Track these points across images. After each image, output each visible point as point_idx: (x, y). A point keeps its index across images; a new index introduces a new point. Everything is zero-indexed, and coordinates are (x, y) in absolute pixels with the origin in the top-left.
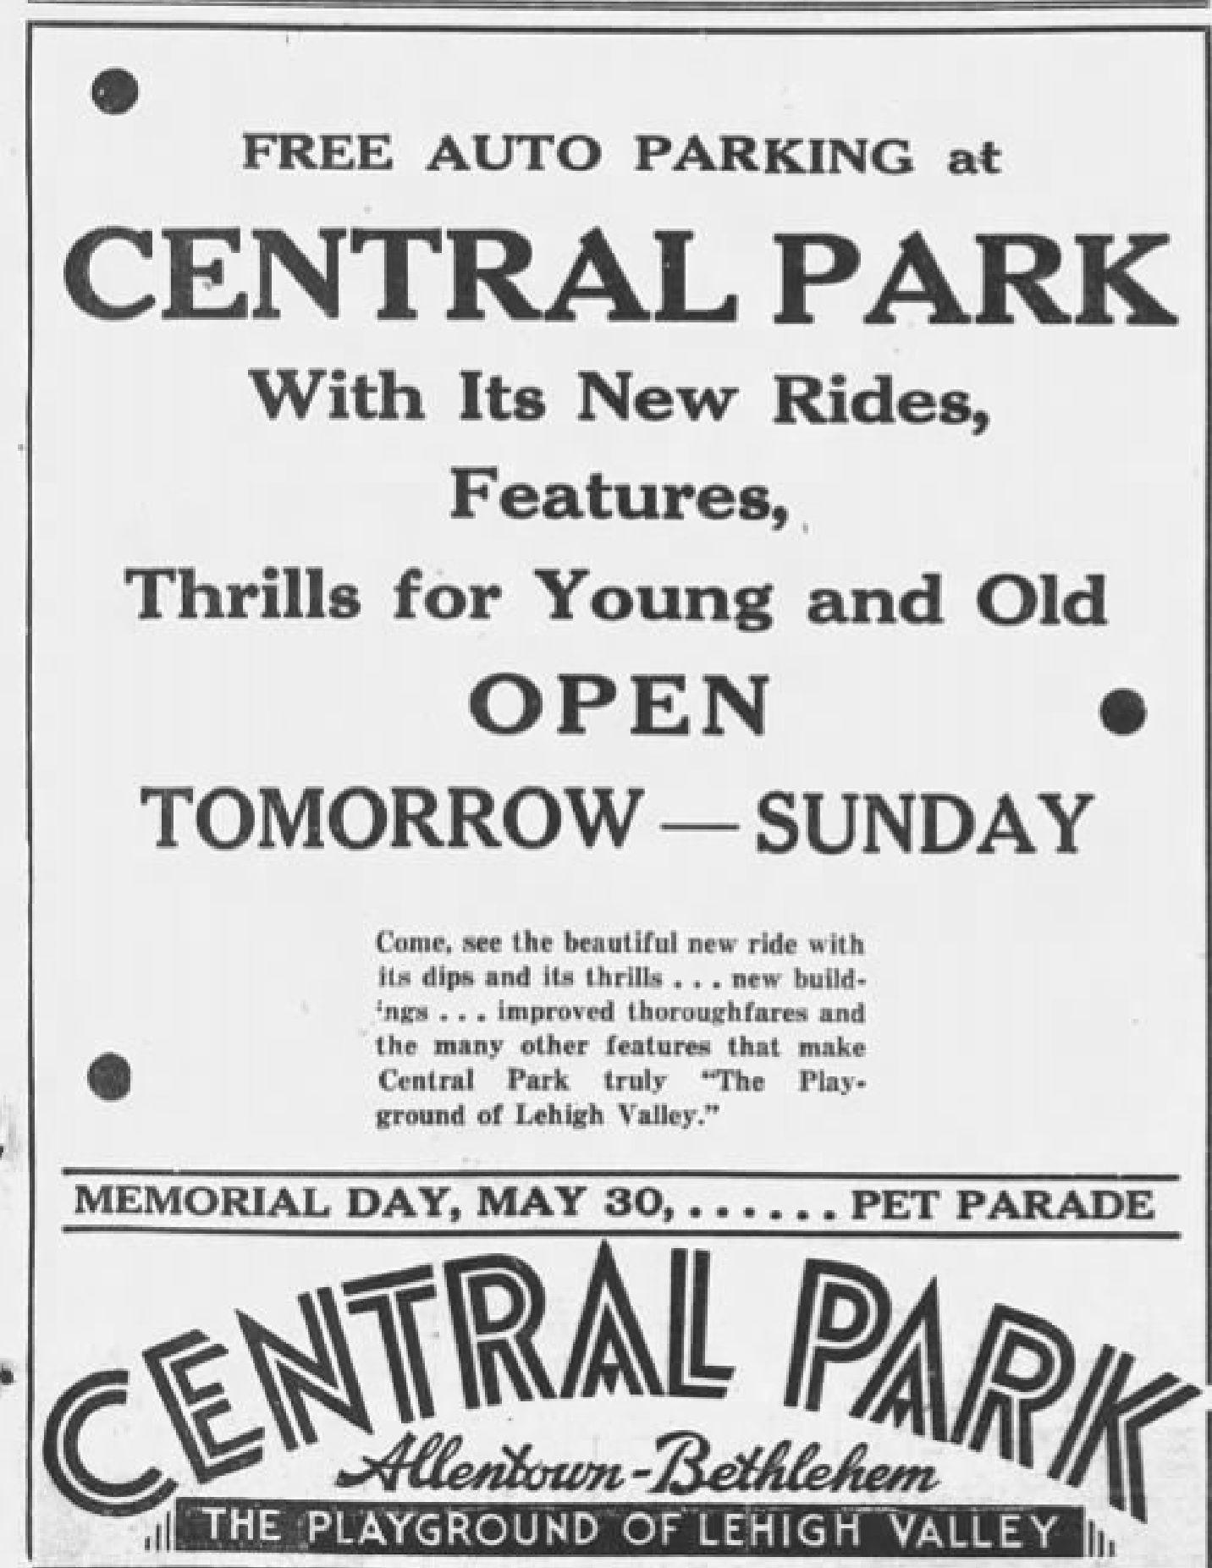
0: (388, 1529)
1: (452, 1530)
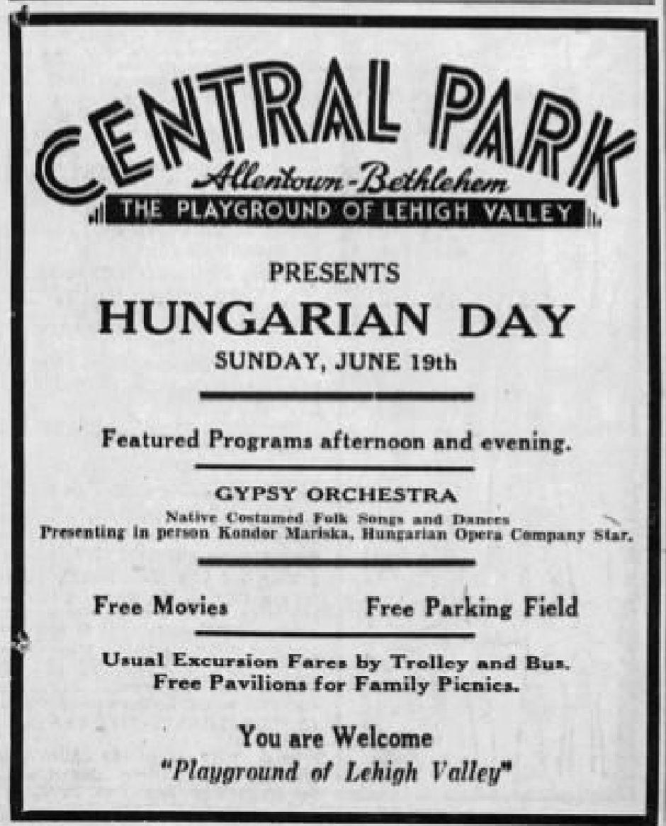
0: (220, 210)
1: (253, 210)
